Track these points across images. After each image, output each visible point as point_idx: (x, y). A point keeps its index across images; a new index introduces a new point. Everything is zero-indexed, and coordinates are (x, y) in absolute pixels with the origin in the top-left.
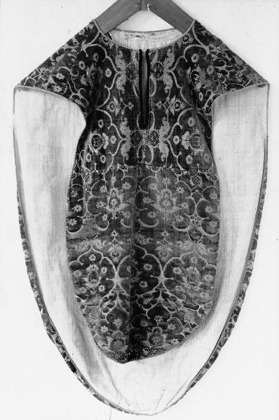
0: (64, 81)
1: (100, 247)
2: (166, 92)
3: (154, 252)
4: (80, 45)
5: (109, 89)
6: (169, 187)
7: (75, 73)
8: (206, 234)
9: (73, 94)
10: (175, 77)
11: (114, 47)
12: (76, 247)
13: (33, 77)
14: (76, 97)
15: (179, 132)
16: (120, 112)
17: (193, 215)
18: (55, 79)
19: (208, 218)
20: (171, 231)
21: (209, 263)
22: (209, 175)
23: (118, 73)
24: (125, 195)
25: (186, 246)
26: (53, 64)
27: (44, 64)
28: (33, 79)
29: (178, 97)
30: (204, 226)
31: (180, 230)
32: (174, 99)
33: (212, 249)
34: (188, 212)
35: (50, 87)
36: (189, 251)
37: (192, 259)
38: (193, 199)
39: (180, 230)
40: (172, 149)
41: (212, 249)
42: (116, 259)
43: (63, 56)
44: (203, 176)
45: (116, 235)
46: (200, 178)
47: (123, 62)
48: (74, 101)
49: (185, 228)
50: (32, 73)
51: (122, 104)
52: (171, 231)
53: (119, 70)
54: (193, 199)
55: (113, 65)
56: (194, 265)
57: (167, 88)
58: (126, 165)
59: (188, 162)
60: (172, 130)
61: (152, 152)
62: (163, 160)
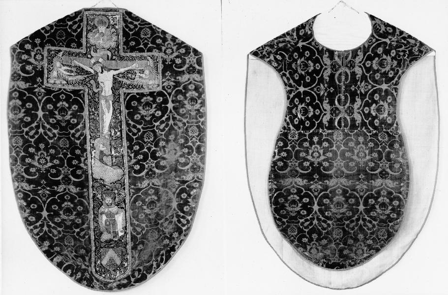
0: (281, 61)
1: (301, 184)
2: (357, 79)
3: (354, 190)
4: (298, 42)
5: (317, 77)
6: (363, 143)
7: (289, 58)
8: (392, 173)
9: (284, 72)
10: (363, 68)
11: (323, 49)
12: (282, 182)
13: (259, 51)
14: (284, 75)
15: (368, 105)
16: (324, 93)
17: (382, 161)
18: (275, 58)
19: (393, 162)
20: (366, 174)
21: (396, 193)
22: (391, 132)
23: (325, 67)
24: (324, 151)
25: (378, 182)
26: (276, 47)
27: (270, 45)
28: (259, 52)
29: (367, 81)
30: (391, 167)
31: (372, 172)
32: (363, 83)
33: (397, 183)
34: (378, 159)
35: (270, 62)
36: (379, 187)
37: (382, 192)
38: (381, 150)
39: (372, 172)
40: (363, 116)
41: (397, 183)
42: (316, 194)
43: (284, 44)
44: (387, 133)
45: (317, 177)
46: (386, 134)
47: (329, 60)
48: (282, 77)
49: (376, 170)
50: (260, 47)
51: (326, 88)
52: (366, 174)
53: (326, 65)
54: (381, 150)
55: (321, 60)
56: (384, 196)
57: (358, 76)
58: (325, 130)
59: (376, 125)
60: (363, 104)
61: (349, 120)
62: (357, 125)
